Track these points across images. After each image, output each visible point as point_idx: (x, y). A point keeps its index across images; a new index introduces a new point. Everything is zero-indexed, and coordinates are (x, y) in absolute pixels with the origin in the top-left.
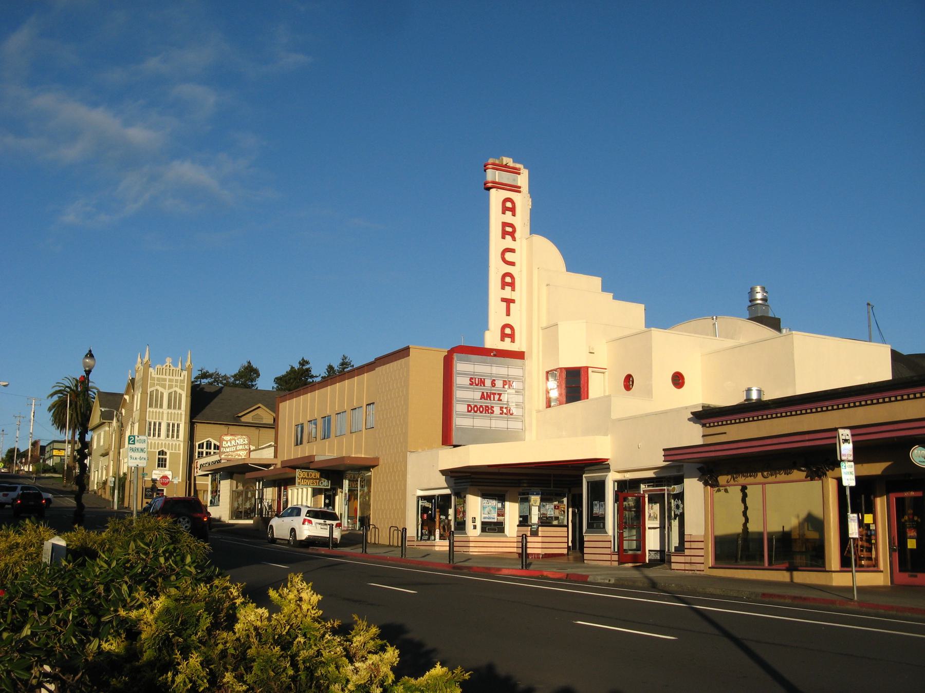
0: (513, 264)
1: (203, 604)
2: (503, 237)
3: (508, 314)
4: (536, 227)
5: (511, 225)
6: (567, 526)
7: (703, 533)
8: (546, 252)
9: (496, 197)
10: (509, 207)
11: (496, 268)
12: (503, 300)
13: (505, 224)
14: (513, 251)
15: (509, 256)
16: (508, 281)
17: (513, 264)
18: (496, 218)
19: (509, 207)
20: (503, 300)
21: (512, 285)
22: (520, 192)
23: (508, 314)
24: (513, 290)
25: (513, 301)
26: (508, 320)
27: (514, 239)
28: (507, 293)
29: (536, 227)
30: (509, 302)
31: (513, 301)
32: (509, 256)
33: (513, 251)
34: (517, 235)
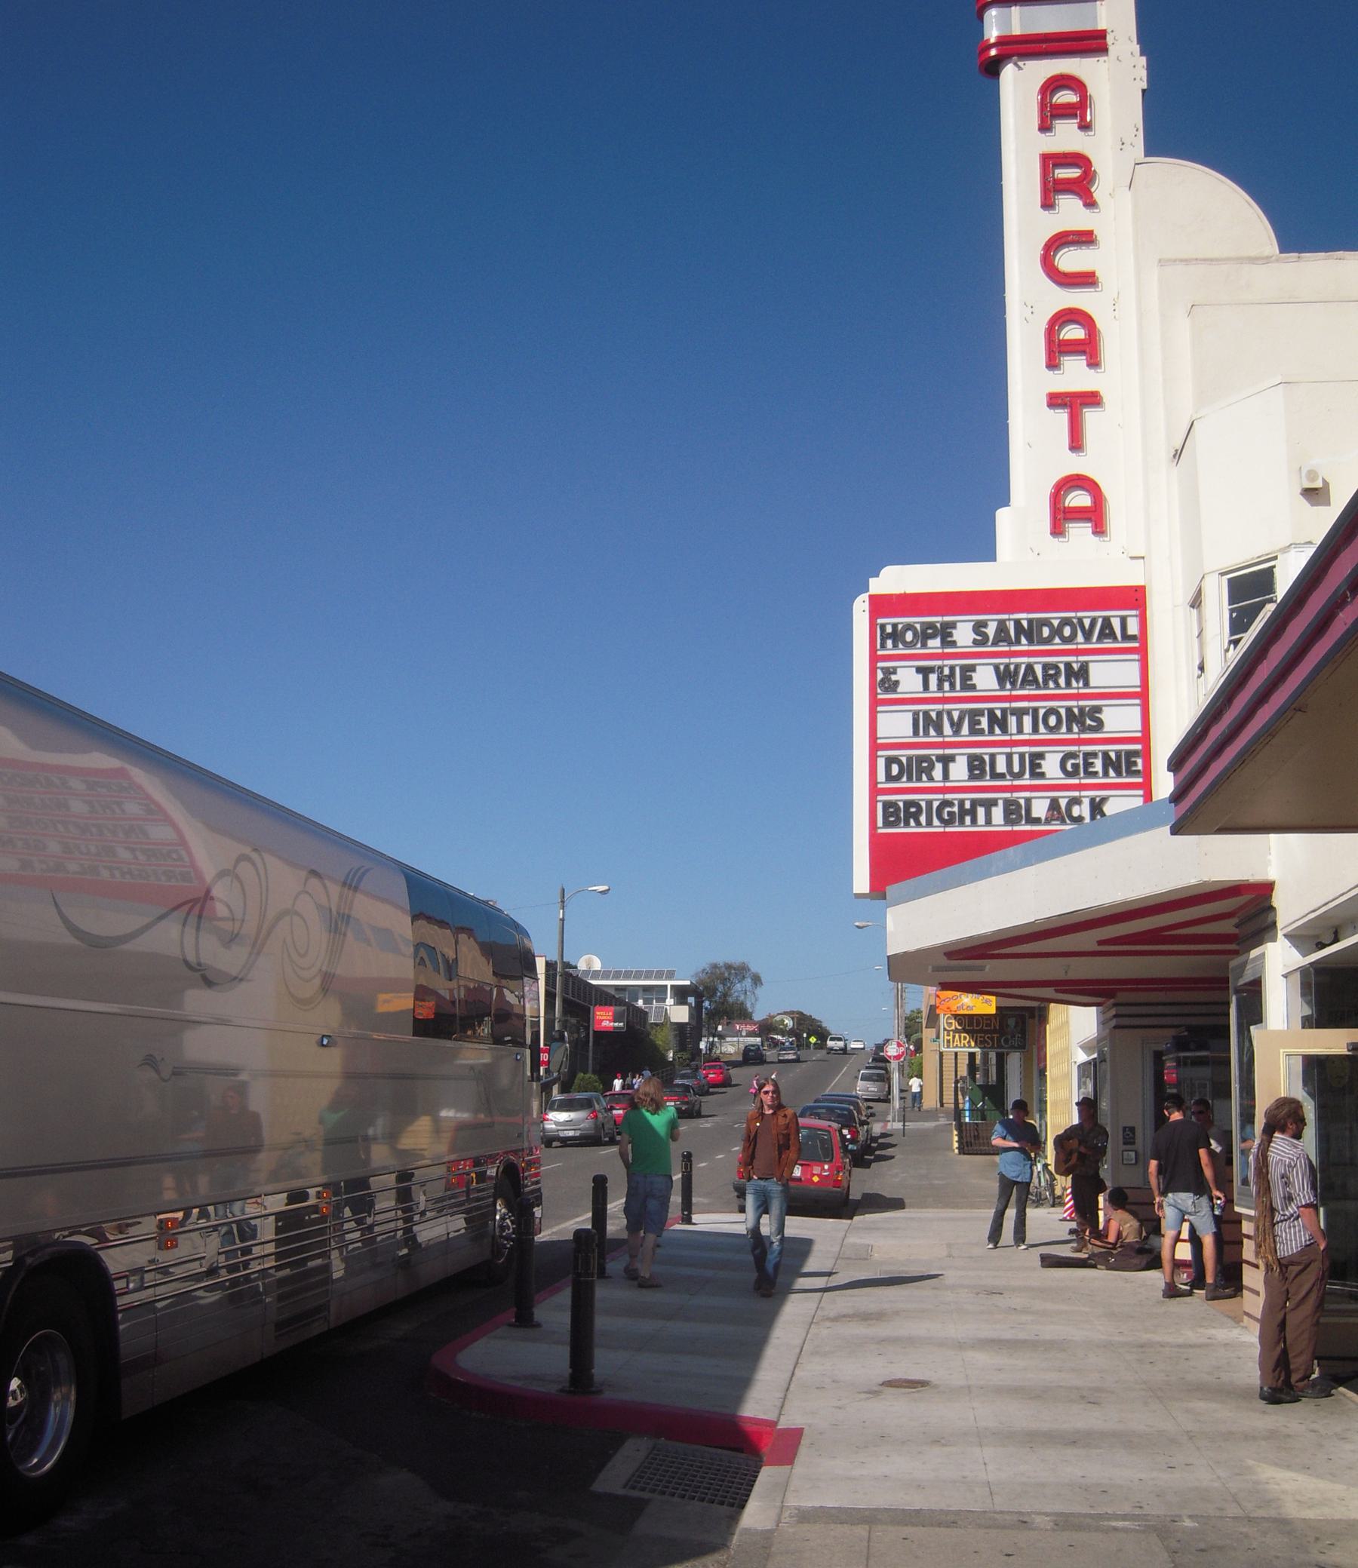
0: (1086, 280)
1: (441, 1171)
2: (1057, 530)
3: (1076, 443)
4: (1168, 131)
5: (1079, 160)
6: (875, 746)
7: (1094, 1009)
8: (1214, 207)
9: (1019, 87)
10: (1064, 103)
11: (1028, 300)
12: (1056, 400)
13: (1051, 161)
14: (1084, 238)
15: (1069, 260)
16: (1073, 338)
17: (1086, 280)
18: (1021, 144)
19: (1064, 103)
20: (1056, 400)
21: (1089, 349)
22: (1103, 50)
23: (1076, 443)
24: (1094, 363)
25: (1092, 399)
26: (1075, 465)
27: (1090, 203)
28: (1074, 375)
29: (1168, 131)
30: (1075, 405)
31: (1092, 399)
32: (1069, 260)
33: (1084, 238)
34: (1099, 191)
